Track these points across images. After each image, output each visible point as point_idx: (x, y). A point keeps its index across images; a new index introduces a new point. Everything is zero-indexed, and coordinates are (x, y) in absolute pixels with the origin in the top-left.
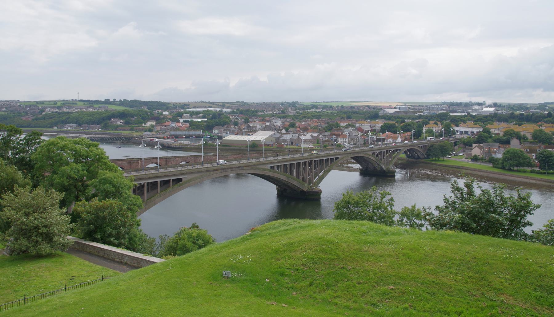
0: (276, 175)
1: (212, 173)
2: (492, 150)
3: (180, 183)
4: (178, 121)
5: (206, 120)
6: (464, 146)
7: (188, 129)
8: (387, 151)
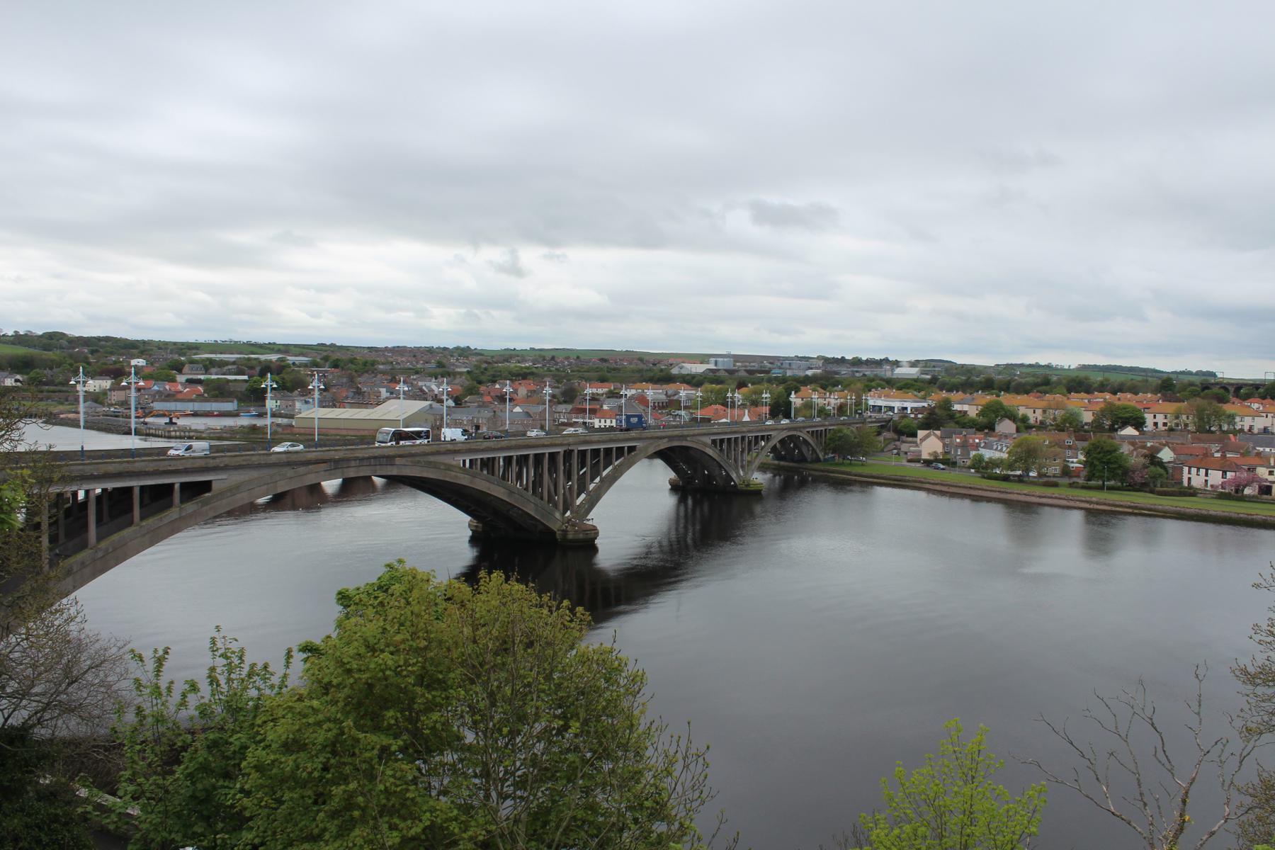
0: (483, 484)
1: (302, 470)
2: (971, 441)
3: (207, 495)
4: (173, 380)
5: (246, 377)
6: (896, 437)
7: (201, 398)
8: (743, 438)
